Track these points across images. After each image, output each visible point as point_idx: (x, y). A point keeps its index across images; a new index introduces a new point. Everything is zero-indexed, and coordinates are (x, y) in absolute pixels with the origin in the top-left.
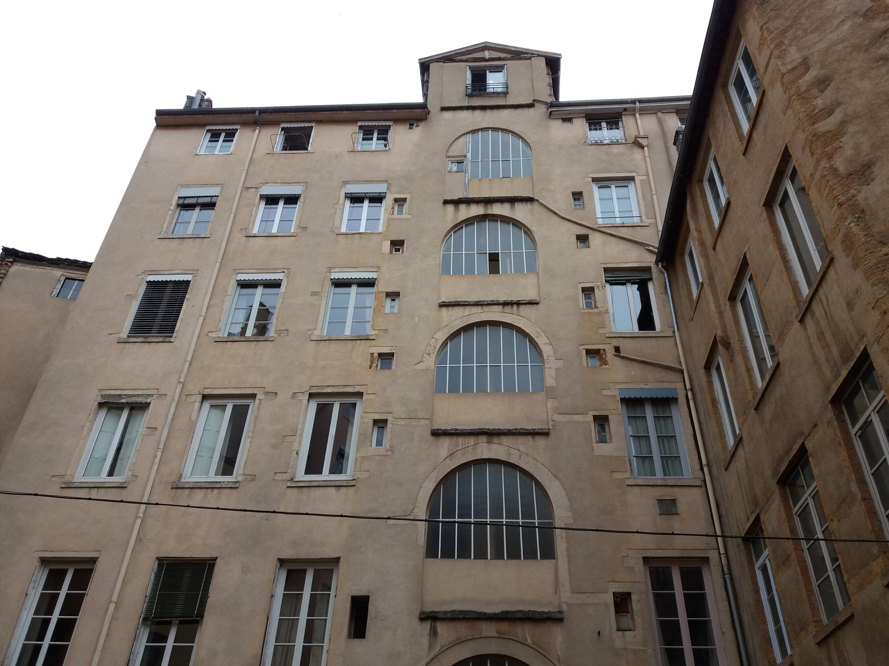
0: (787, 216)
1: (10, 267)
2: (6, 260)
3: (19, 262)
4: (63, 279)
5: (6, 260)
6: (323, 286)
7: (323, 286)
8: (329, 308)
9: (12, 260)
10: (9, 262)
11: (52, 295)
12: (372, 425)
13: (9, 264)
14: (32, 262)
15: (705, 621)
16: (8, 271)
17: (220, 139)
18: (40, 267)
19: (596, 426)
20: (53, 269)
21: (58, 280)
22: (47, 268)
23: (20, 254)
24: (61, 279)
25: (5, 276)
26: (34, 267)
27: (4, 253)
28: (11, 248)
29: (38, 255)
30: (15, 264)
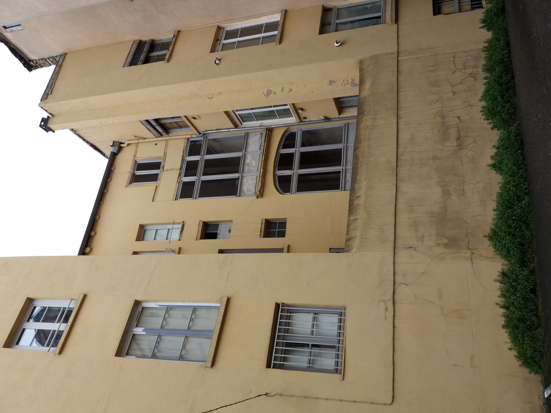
0: (126, 91)
1: (35, 60)
2: (34, 65)
3: (28, 58)
4: (8, 30)
5: (34, 65)
6: (466, 106)
7: (466, 106)
8: (313, 336)
9: (31, 62)
10: (34, 63)
11: (23, 28)
12: (243, 197)
13: (34, 62)
14: (19, 52)
15: (265, 25)
16: (39, 59)
17: (251, 112)
18: (17, 46)
19: (295, 354)
20: (9, 39)
21: (11, 32)
22: (13, 42)
23: (23, 62)
24: (9, 31)
25: (43, 59)
26: (21, 49)
27: (32, 69)
28: (26, 69)
29: (13, 53)
30: (31, 59)
